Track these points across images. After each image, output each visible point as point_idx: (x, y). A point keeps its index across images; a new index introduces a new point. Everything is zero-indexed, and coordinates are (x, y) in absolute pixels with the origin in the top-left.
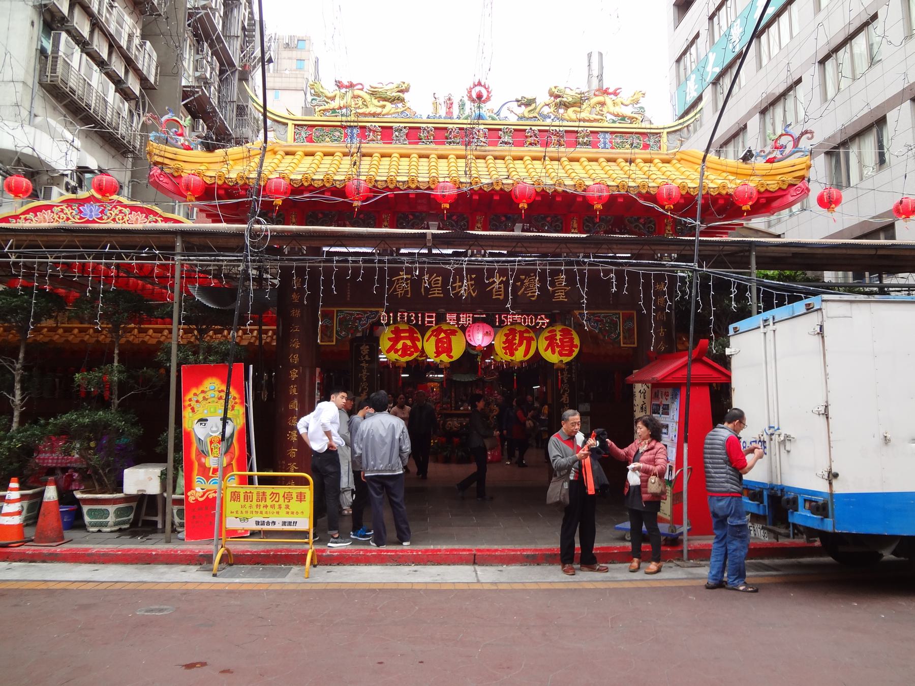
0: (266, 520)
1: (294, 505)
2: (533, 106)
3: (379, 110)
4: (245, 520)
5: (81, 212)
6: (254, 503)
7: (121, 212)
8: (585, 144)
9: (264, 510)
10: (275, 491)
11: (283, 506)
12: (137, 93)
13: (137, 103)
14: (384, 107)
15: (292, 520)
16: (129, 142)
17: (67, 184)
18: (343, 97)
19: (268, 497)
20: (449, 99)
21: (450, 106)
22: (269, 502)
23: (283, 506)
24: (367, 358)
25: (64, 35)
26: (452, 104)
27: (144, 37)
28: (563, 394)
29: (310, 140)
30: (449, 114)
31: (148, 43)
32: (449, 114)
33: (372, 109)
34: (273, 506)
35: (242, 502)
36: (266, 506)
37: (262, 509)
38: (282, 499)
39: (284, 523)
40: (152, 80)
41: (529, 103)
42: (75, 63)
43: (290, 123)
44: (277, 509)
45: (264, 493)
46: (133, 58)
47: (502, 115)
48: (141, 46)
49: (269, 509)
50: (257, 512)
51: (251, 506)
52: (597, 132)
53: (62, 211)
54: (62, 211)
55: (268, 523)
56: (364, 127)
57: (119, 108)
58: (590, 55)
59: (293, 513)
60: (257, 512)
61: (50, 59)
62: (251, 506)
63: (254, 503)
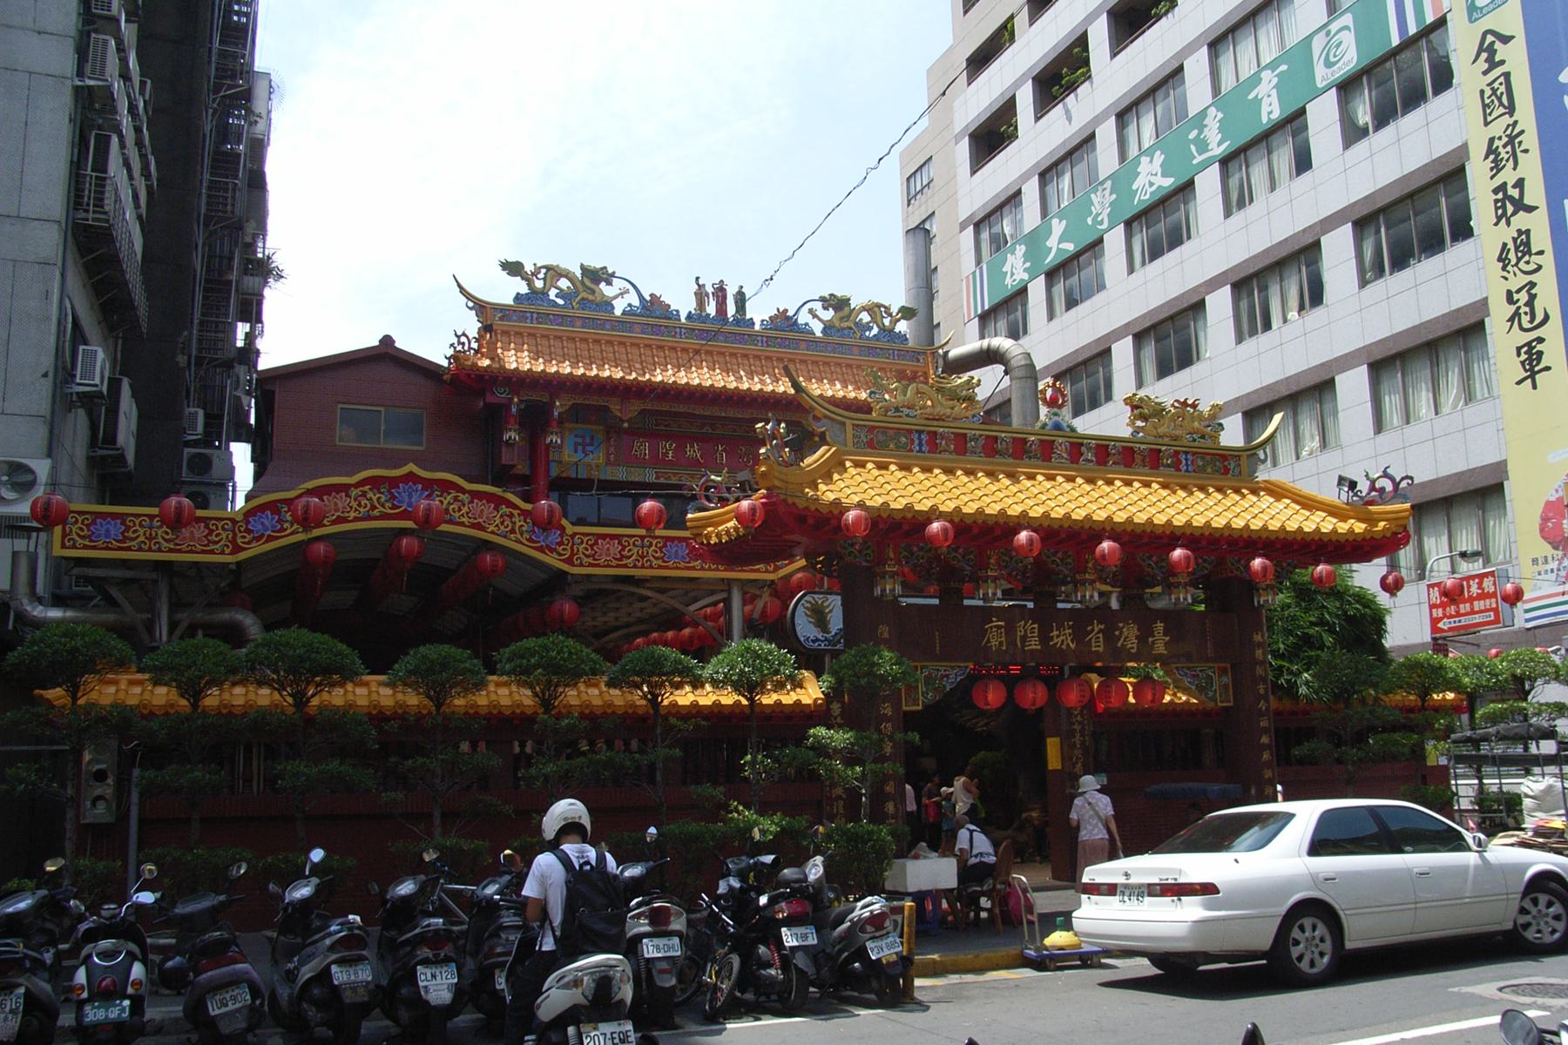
5: (394, 497)
7: (456, 499)
26: (725, 297)
53: (364, 494)
54: (364, 494)
56: (935, 433)
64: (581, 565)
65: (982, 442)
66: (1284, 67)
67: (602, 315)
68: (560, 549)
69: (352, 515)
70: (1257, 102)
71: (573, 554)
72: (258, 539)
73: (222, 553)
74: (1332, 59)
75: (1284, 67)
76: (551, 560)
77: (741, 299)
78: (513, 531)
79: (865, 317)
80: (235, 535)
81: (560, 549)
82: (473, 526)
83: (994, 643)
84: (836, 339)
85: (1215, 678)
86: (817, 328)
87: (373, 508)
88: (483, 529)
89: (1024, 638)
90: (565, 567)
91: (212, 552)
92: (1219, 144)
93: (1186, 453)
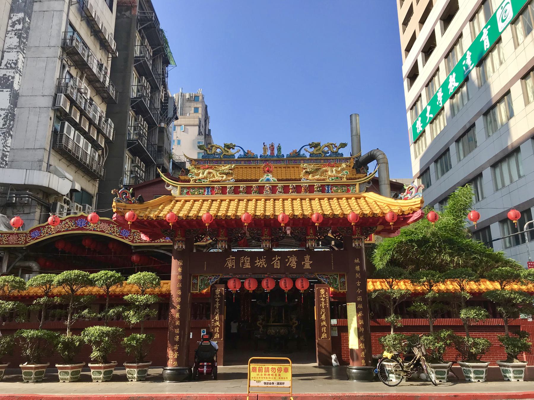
0: (269, 382)
1: (283, 374)
2: (319, 147)
3: (220, 179)
4: (259, 382)
6: (263, 373)
8: (318, 191)
9: (268, 377)
10: (273, 367)
11: (278, 375)
12: (103, 146)
13: (103, 152)
14: (223, 177)
15: (282, 382)
16: (98, 173)
17: (65, 199)
18: (203, 173)
19: (270, 370)
20: (272, 146)
21: (272, 150)
22: (270, 373)
23: (278, 375)
24: (219, 296)
25: (67, 123)
26: (274, 148)
27: (107, 116)
28: (322, 314)
29: (187, 193)
30: (272, 153)
31: (110, 120)
32: (272, 153)
33: (217, 178)
34: (272, 375)
35: (257, 373)
36: (269, 375)
37: (267, 376)
38: (277, 371)
39: (278, 384)
40: (111, 139)
41: (315, 145)
42: (71, 137)
43: (179, 186)
44: (274, 376)
45: (268, 368)
46: (101, 128)
47: (302, 153)
48: (106, 122)
49: (270, 376)
50: (264, 378)
51: (262, 375)
52: (324, 185)
53: (114, 227)
55: (270, 384)
56: (214, 187)
57: (93, 155)
58: (483, 198)
59: (282, 378)
60: (264, 378)
61: (59, 135)
62: (262, 375)
63: (263, 373)
64: (136, 243)
65: (233, 188)
66: (489, 27)
67: (232, 159)
68: (129, 238)
69: (63, 230)
70: (483, 42)
71: (134, 239)
72: (33, 239)
73: (22, 244)
74: (504, 18)
75: (489, 27)
76: (126, 241)
77: (279, 149)
78: (114, 232)
79: (326, 149)
80: (26, 238)
81: (129, 238)
82: (101, 231)
83: (230, 265)
84: (314, 158)
85: (338, 279)
86: (308, 155)
87: (69, 227)
88: (104, 232)
89: (243, 263)
90: (130, 243)
91: (18, 244)
92: (471, 65)
93: (328, 185)
